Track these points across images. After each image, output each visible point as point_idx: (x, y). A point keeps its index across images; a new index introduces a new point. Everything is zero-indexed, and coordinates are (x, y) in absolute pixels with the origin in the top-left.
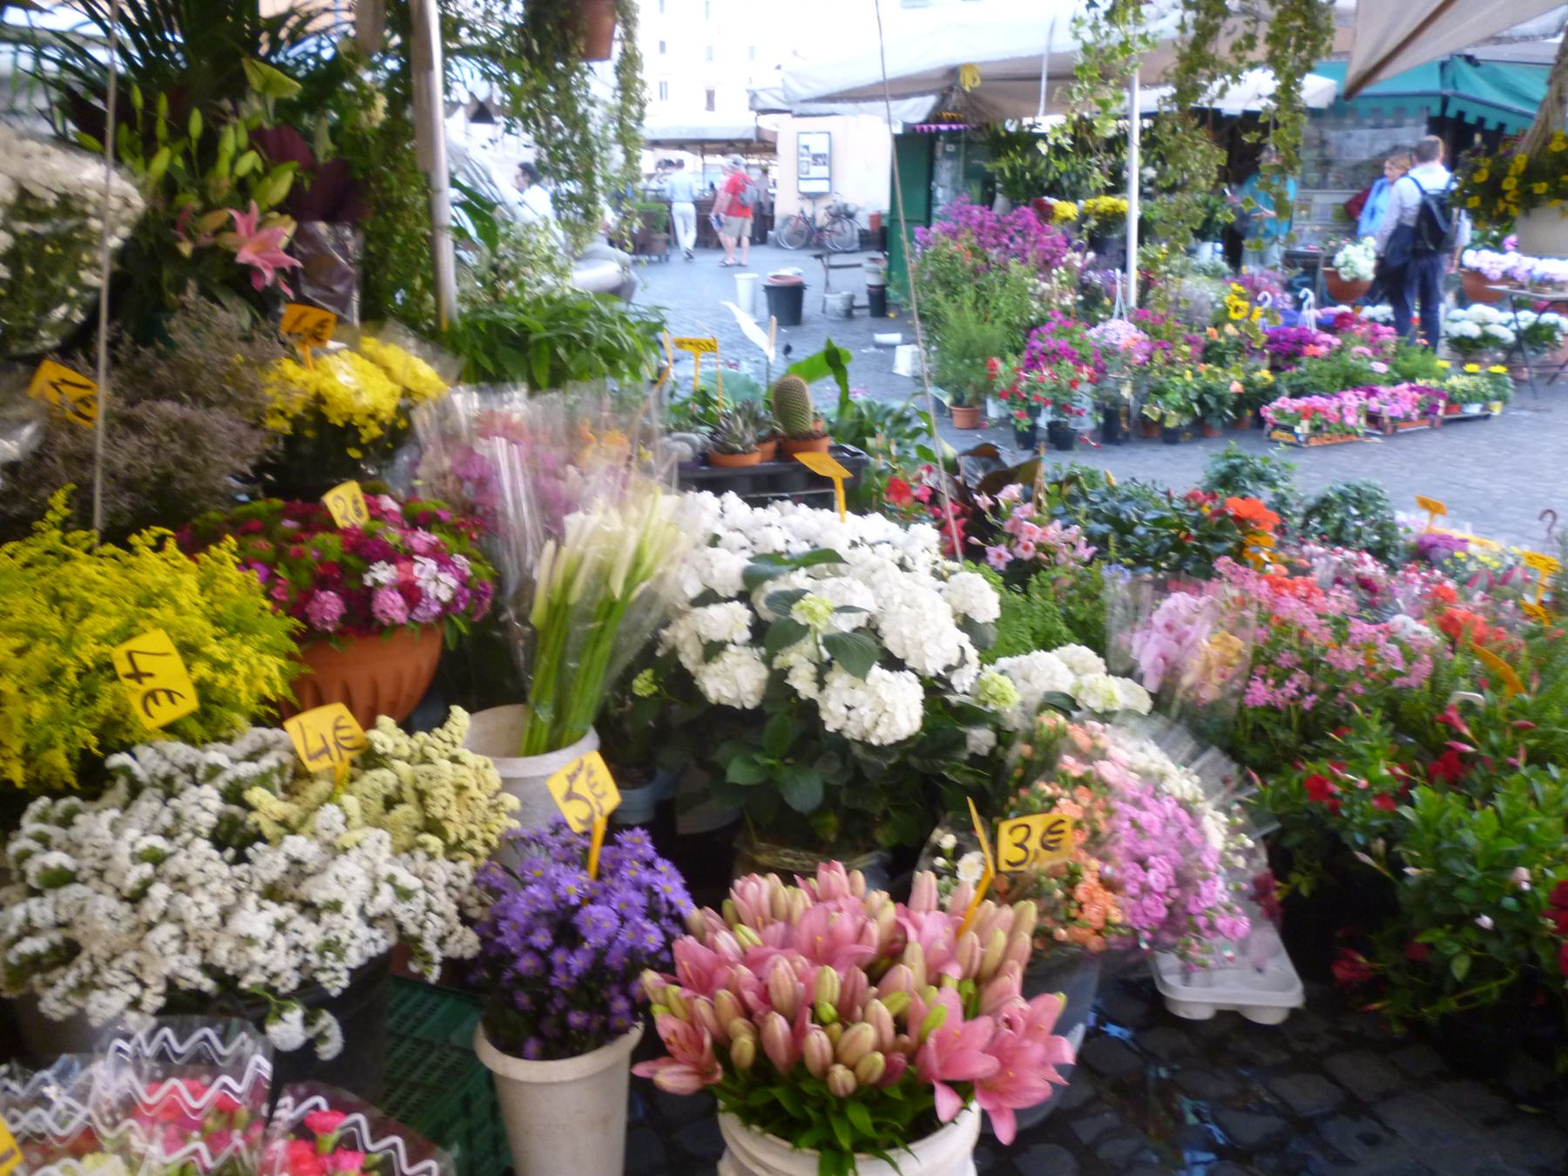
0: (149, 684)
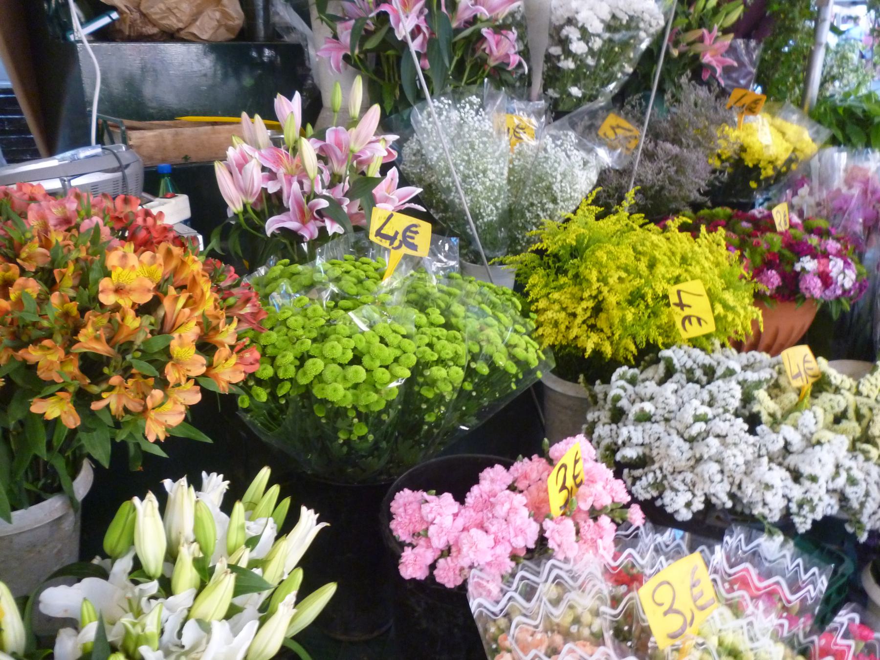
0: (687, 311)
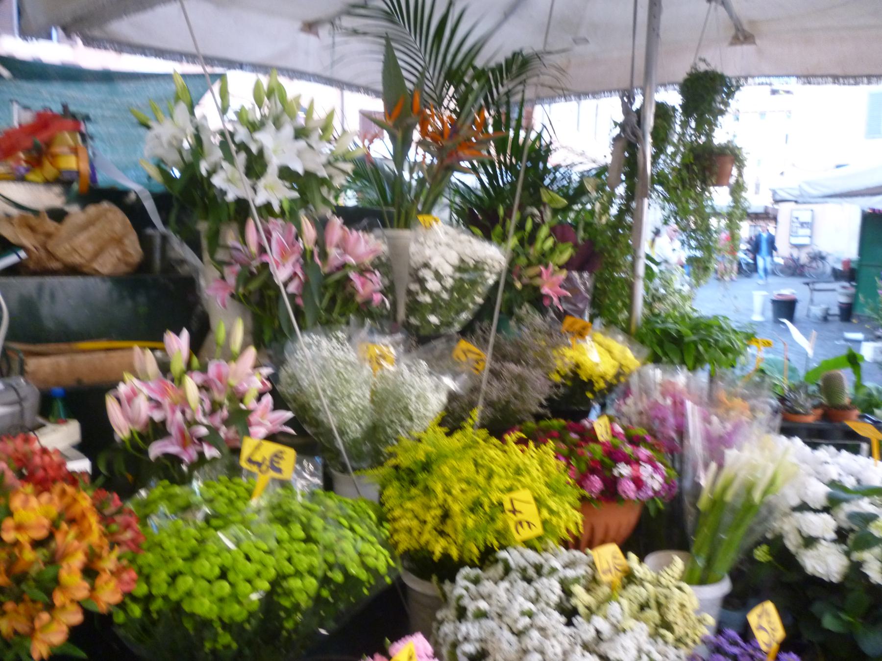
0: (519, 517)
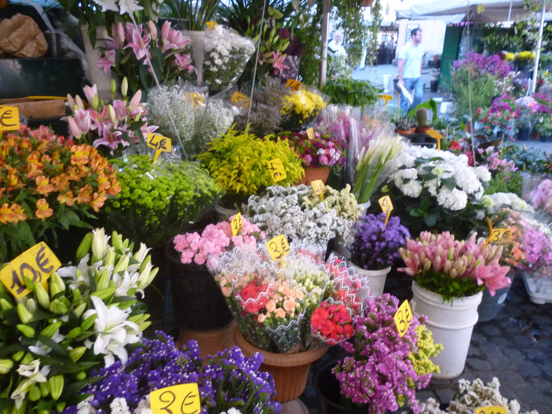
0: (275, 171)
